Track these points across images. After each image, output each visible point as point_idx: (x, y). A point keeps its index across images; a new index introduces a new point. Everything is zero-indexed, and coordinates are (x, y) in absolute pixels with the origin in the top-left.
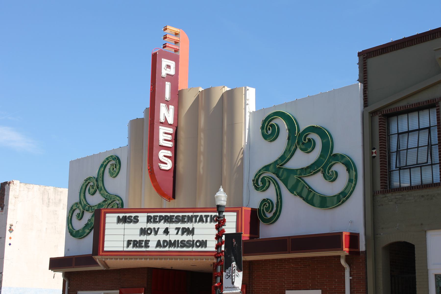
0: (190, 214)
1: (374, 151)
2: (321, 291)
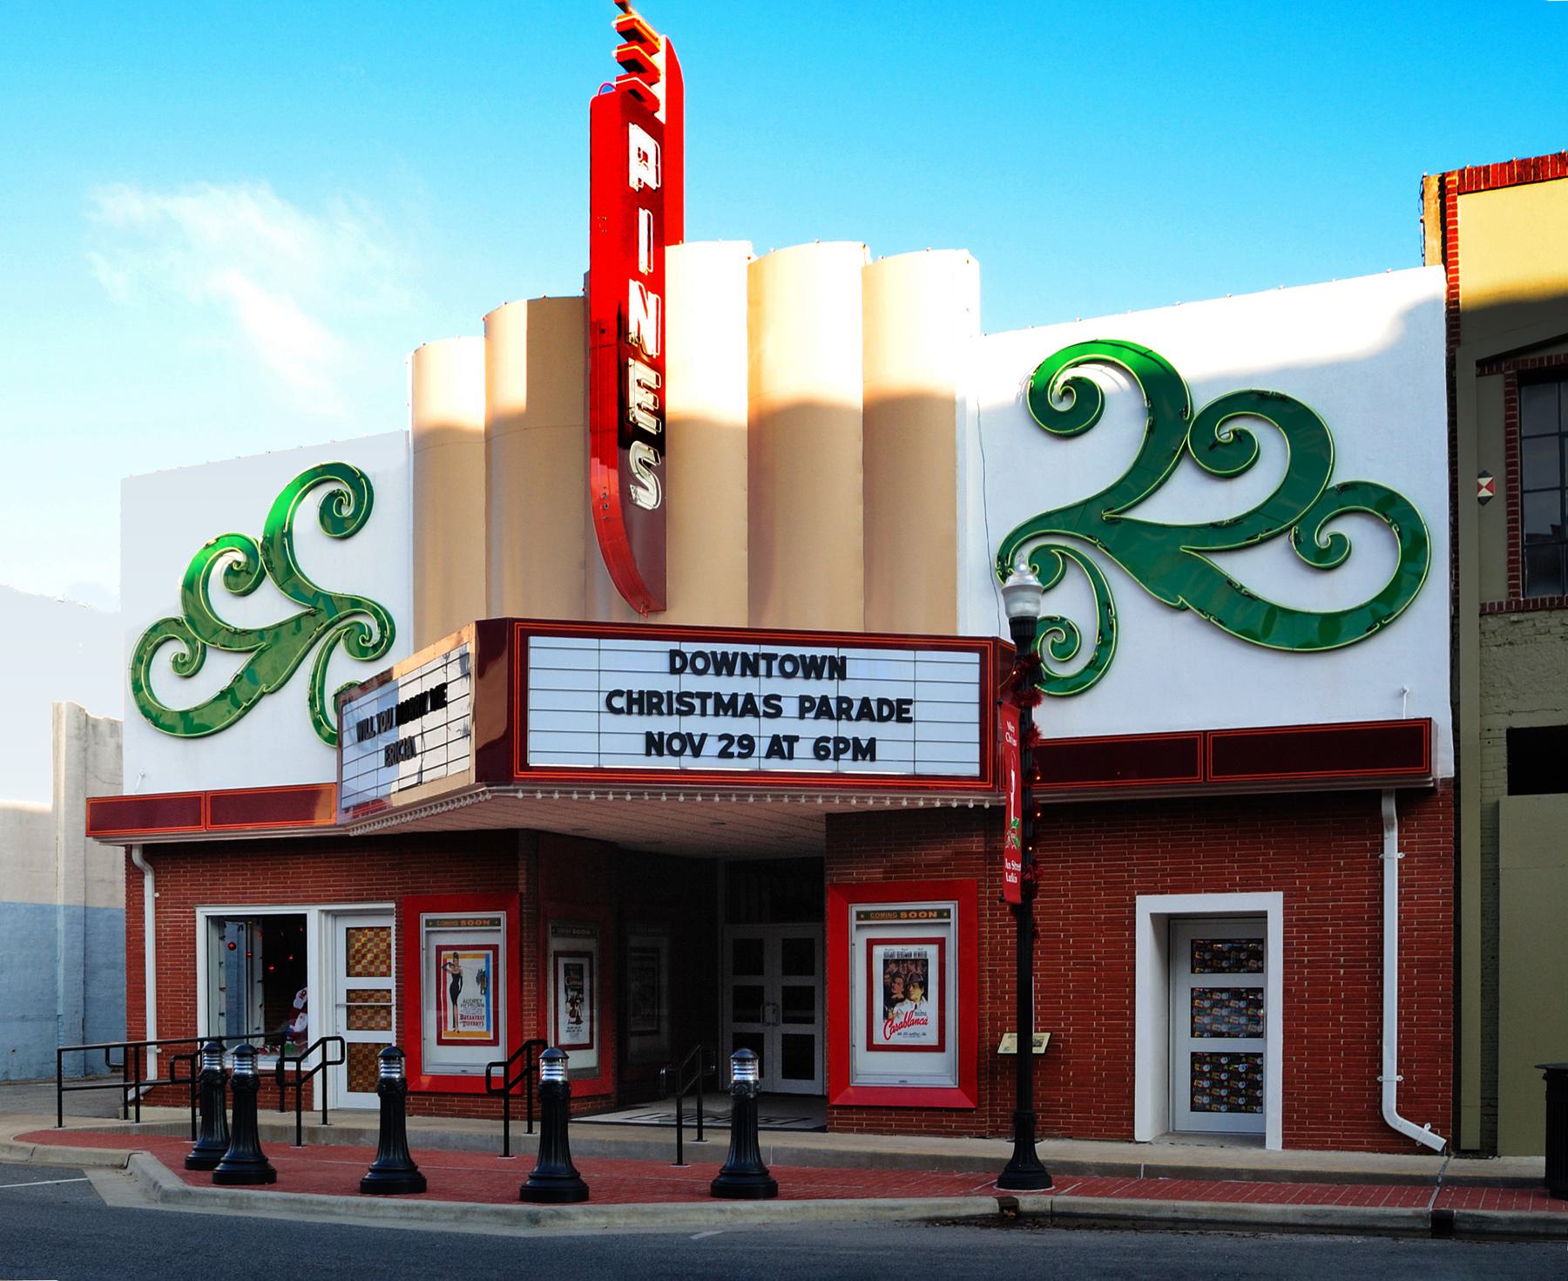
0: (751, 649)
1: (1484, 481)
2: (1281, 894)
